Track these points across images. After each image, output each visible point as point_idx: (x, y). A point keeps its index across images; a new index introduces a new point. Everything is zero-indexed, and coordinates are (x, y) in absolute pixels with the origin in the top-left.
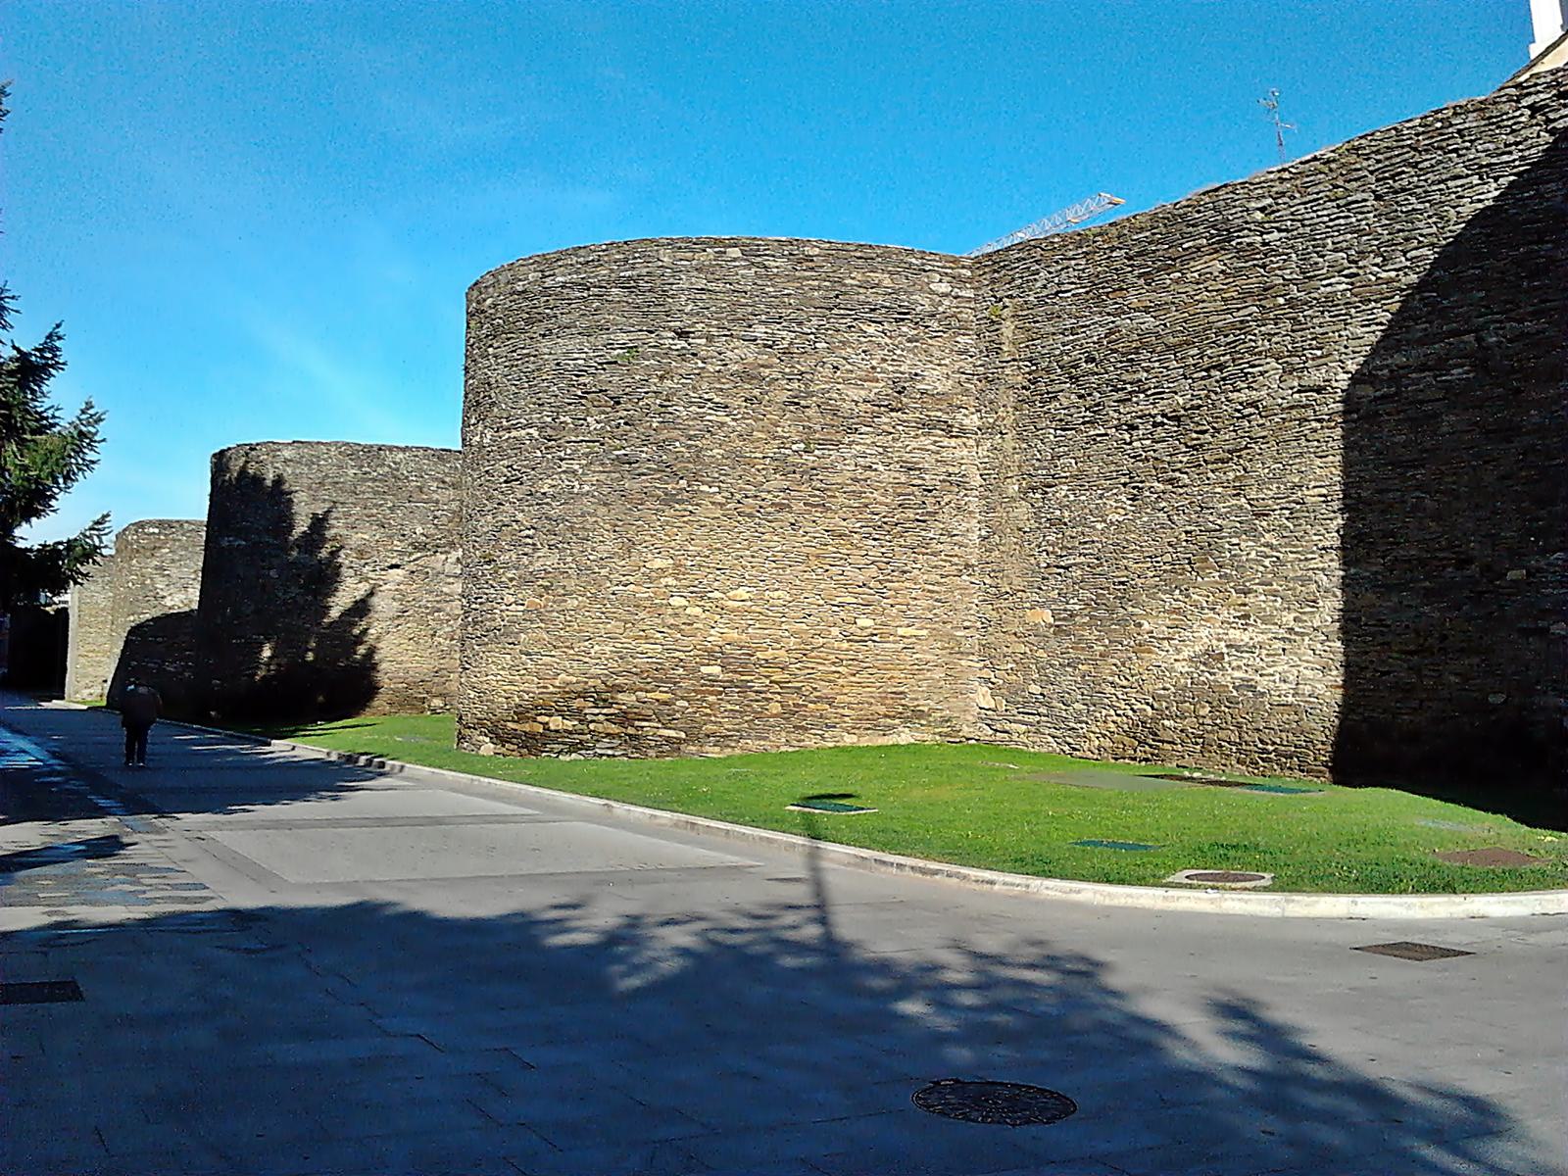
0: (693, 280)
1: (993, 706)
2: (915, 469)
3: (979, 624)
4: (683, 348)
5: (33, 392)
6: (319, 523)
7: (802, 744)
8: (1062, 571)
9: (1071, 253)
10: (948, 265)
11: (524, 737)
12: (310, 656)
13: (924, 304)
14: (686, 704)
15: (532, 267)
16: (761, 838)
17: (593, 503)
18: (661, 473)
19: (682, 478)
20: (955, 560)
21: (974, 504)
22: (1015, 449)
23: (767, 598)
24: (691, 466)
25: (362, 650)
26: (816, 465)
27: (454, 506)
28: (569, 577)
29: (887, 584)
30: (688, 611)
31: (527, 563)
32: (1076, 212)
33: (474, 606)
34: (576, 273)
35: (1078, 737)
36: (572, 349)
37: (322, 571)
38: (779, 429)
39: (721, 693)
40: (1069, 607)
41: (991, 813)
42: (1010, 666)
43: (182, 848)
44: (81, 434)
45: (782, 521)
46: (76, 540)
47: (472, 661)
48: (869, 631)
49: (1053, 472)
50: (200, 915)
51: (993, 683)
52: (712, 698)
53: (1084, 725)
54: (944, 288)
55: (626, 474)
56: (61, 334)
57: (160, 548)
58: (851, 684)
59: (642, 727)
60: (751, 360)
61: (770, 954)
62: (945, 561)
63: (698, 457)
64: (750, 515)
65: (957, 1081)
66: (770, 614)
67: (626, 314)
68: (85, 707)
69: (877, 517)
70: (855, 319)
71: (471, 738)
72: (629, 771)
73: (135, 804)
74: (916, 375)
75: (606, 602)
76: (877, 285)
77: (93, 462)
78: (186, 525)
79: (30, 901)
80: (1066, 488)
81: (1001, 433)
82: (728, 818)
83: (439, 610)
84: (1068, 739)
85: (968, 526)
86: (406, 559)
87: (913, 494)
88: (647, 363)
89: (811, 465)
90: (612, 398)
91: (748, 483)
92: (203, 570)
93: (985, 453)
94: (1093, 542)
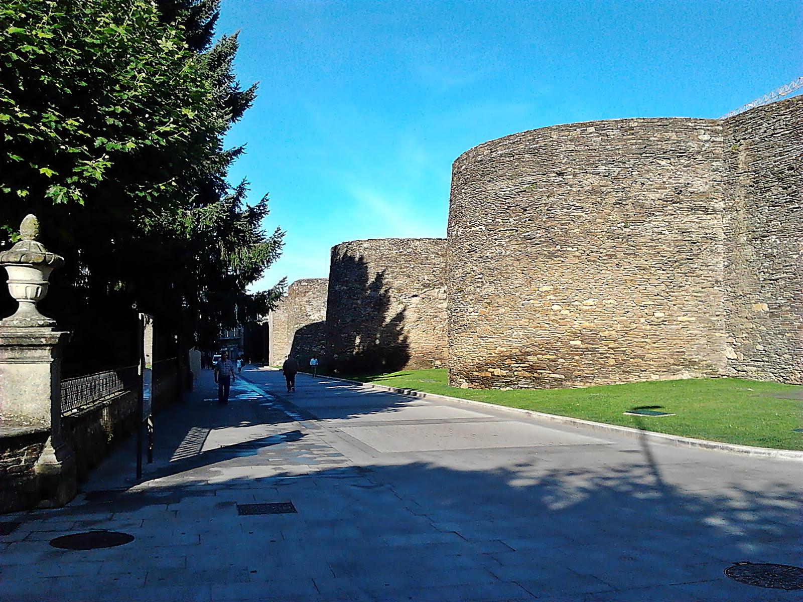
1: (736, 358)
2: (687, 232)
3: (725, 313)
4: (560, 181)
5: (255, 225)
6: (380, 277)
7: (628, 380)
8: (772, 282)
9: (782, 112)
10: (709, 125)
11: (482, 379)
12: (378, 342)
13: (694, 146)
14: (564, 361)
15: (486, 148)
16: (612, 430)
17: (511, 260)
18: (547, 242)
19: (557, 245)
20: (710, 279)
21: (720, 248)
22: (745, 218)
23: (604, 304)
24: (563, 238)
25: (401, 338)
26: (630, 233)
27: (443, 265)
28: (500, 297)
29: (671, 294)
30: (562, 312)
31: (479, 291)
32: (785, 89)
33: (453, 314)
34: (508, 148)
35: (787, 372)
36: (503, 187)
37: (381, 299)
38: (610, 217)
39: (582, 355)
40: (777, 301)
41: (741, 415)
42: (744, 335)
43: (329, 437)
44: (275, 242)
45: (612, 263)
46: (272, 290)
47: (454, 342)
48: (662, 319)
49: (767, 229)
50: (342, 469)
51: (735, 345)
52: (577, 358)
53: (791, 366)
54: (707, 137)
55: (529, 245)
56: (267, 198)
57: (308, 292)
58: (653, 348)
59: (542, 373)
60: (596, 184)
61: (630, 491)
62: (704, 280)
63: (566, 233)
64: (594, 261)
65: (748, 563)
66: (606, 312)
67: (531, 167)
68: (278, 369)
69: (665, 258)
70: (655, 158)
71: (456, 380)
72: (537, 396)
73: (306, 415)
74: (688, 184)
75: (519, 309)
76: (669, 139)
77: (280, 254)
78: (319, 281)
79: (266, 463)
80: (775, 237)
81: (737, 210)
82: (593, 419)
83: (436, 317)
84: (781, 374)
85: (717, 260)
86: (420, 292)
87: (685, 245)
88: (541, 190)
89: (627, 234)
90: (522, 208)
91: (593, 245)
92: (328, 302)
93: (727, 221)
94: (791, 265)
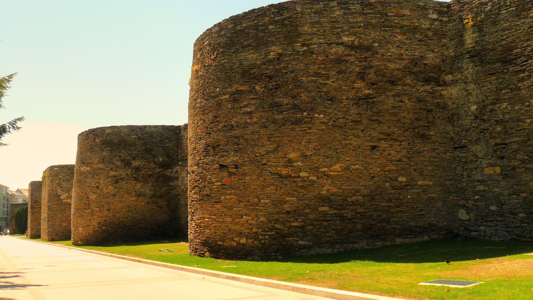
0: (312, 18)
54: (435, 16)
